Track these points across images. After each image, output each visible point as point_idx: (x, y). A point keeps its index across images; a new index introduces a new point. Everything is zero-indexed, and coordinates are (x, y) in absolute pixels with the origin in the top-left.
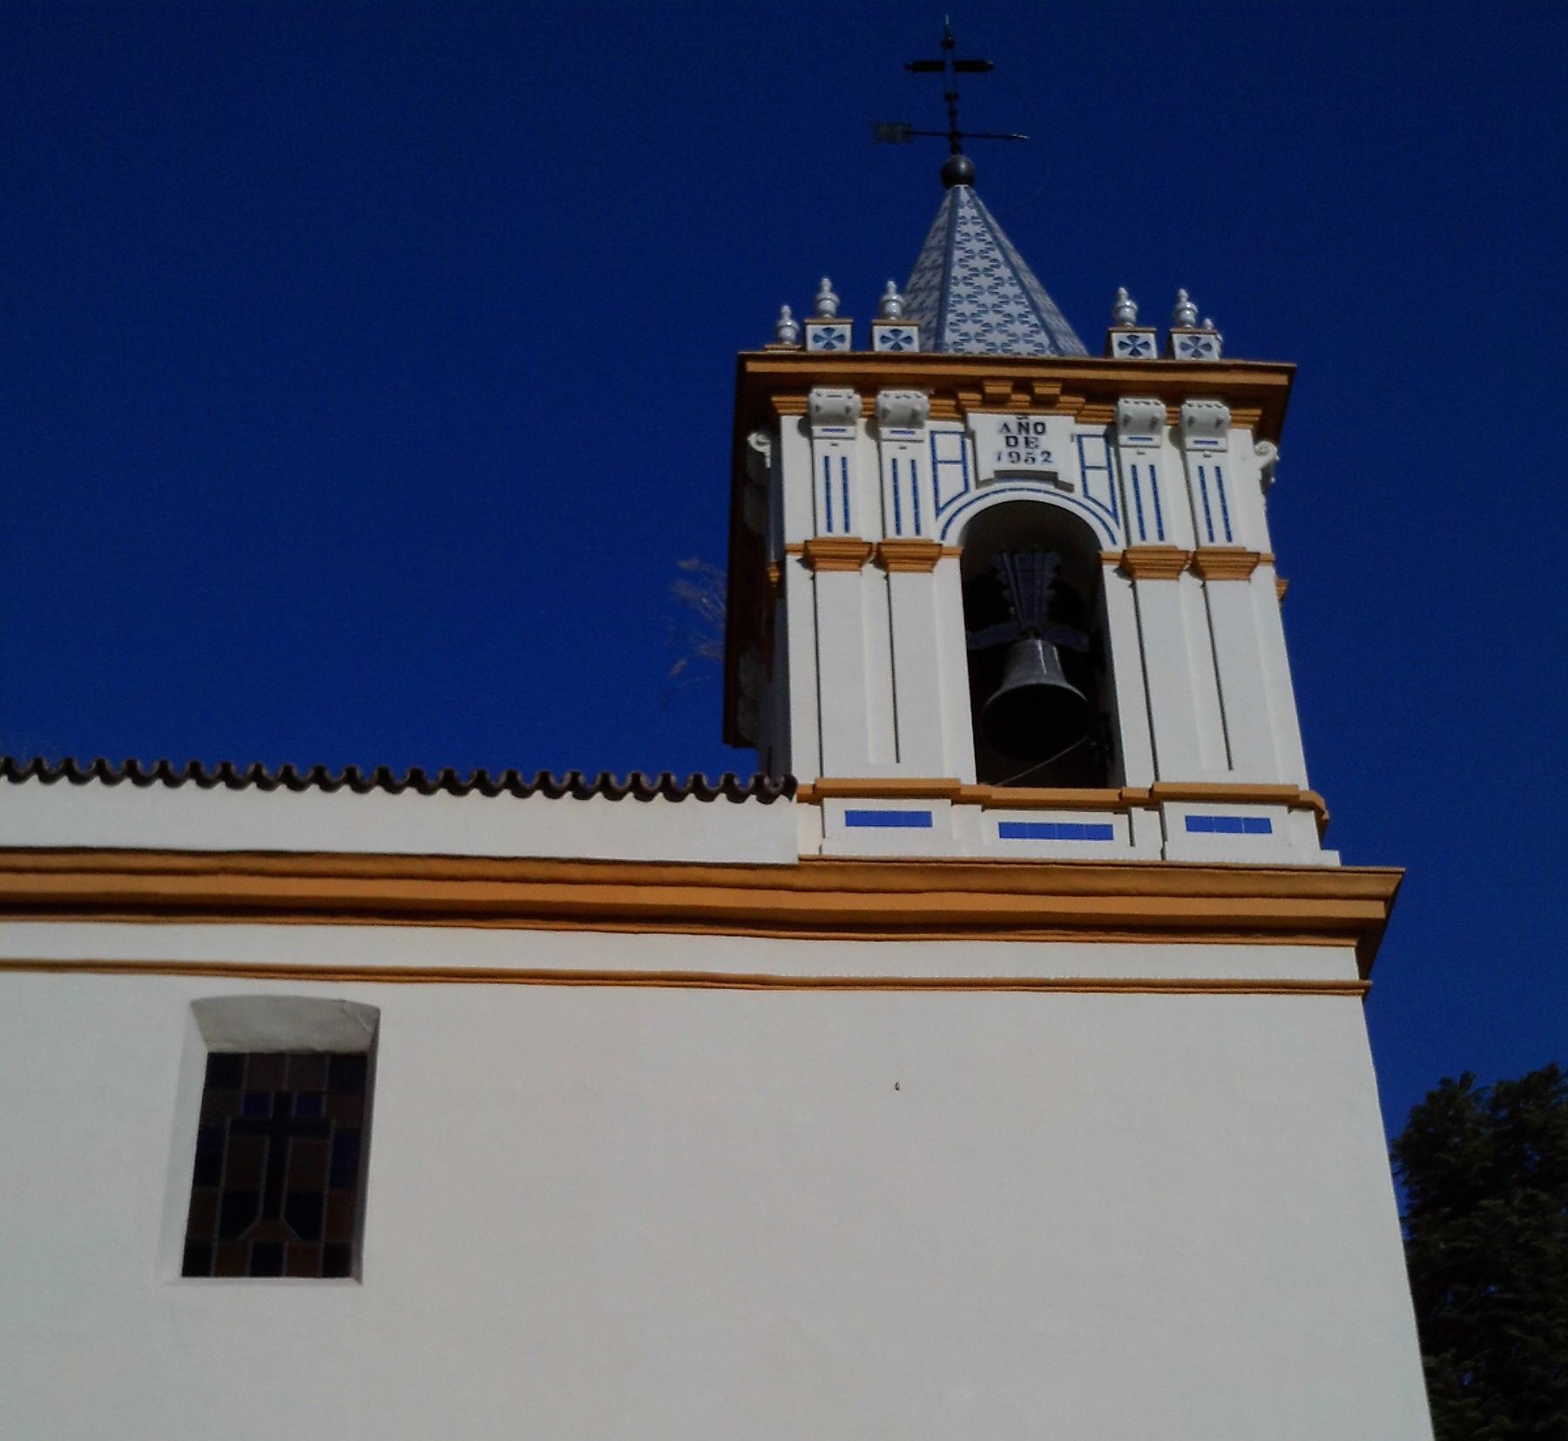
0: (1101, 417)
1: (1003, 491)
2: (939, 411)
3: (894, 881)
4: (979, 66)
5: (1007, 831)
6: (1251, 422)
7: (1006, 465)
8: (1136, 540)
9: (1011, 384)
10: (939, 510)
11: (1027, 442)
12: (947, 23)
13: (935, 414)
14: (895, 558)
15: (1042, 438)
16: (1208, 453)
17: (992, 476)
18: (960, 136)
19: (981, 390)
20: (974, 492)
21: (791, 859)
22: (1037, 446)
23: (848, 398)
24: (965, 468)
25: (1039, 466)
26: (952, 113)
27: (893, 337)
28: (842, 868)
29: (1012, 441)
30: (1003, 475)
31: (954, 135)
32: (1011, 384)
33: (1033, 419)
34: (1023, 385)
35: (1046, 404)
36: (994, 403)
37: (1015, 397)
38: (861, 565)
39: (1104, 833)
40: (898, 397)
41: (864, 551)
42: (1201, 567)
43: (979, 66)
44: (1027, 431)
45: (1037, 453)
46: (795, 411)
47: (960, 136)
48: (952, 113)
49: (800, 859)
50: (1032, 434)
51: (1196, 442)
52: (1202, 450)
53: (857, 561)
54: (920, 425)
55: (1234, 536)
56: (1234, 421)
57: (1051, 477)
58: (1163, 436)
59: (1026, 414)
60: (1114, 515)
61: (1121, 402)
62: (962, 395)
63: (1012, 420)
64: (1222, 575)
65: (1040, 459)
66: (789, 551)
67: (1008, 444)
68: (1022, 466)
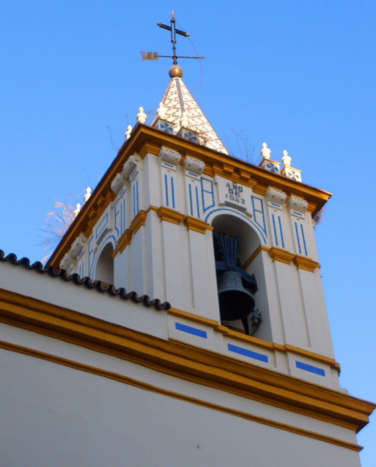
0: (261, 192)
1: (226, 210)
2: (207, 171)
3: (201, 358)
4: (183, 34)
5: (231, 348)
6: (311, 211)
7: (229, 200)
8: (275, 245)
9: (250, 175)
10: (205, 210)
11: (236, 194)
12: (173, 13)
13: (205, 172)
14: (192, 224)
15: (241, 193)
16: (298, 218)
17: (224, 202)
18: (177, 57)
19: (222, 168)
20: (216, 207)
21: (165, 338)
22: (239, 196)
23: (177, 155)
24: (213, 196)
25: (240, 204)
26: (174, 48)
27: (168, 130)
28: (177, 345)
29: (231, 191)
30: (227, 204)
31: (175, 57)
32: (250, 175)
33: (238, 185)
34: (237, 171)
35: (244, 181)
36: (226, 174)
37: (234, 175)
38: (179, 222)
39: (265, 359)
40: (195, 161)
41: (181, 218)
42: (297, 263)
43: (183, 34)
44: (236, 189)
45: (239, 199)
46: (154, 153)
47: (177, 57)
48: (174, 48)
49: (170, 339)
50: (238, 191)
51: (295, 212)
52: (297, 216)
53: (178, 221)
54: (200, 174)
55: (285, 246)
56: (308, 209)
57: (243, 210)
58: (309, 215)
59: (235, 182)
60: (265, 232)
61: (270, 188)
62: (214, 167)
63: (230, 182)
64: (168, 219)
65: (241, 201)
66: (263, 248)
67: (230, 192)
68: (234, 202)
